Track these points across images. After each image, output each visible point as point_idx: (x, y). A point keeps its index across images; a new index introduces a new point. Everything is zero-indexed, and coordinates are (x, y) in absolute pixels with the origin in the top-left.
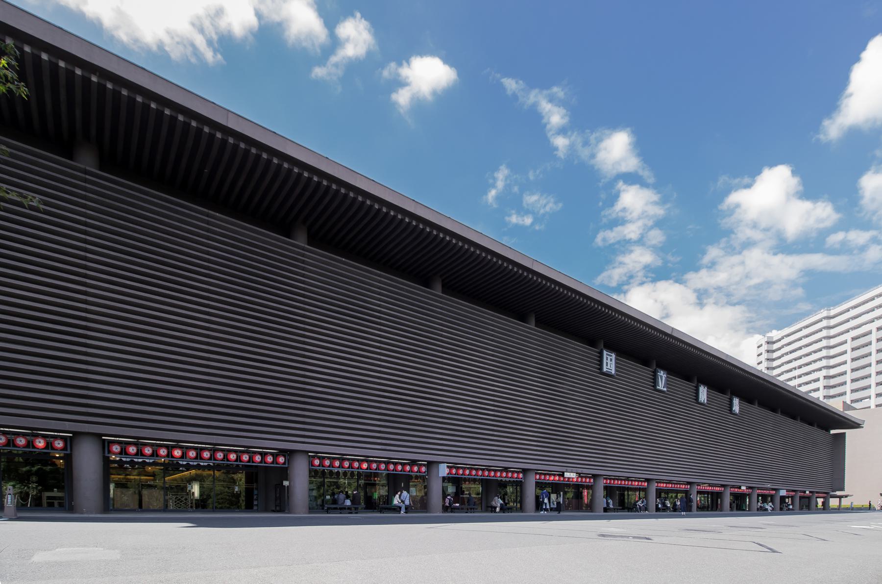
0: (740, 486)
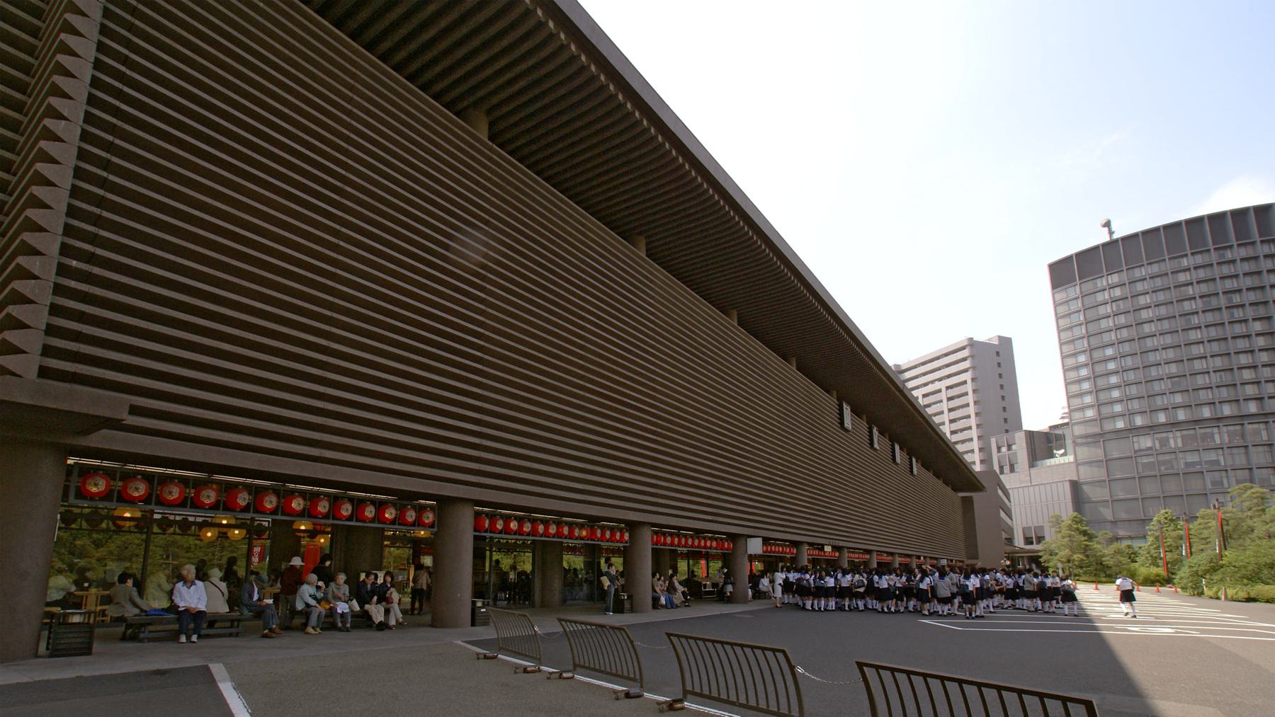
0: (823, 546)
